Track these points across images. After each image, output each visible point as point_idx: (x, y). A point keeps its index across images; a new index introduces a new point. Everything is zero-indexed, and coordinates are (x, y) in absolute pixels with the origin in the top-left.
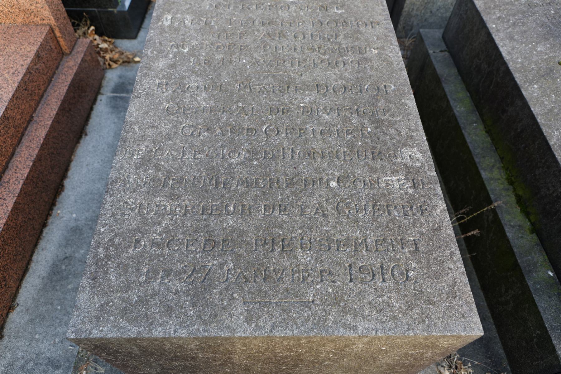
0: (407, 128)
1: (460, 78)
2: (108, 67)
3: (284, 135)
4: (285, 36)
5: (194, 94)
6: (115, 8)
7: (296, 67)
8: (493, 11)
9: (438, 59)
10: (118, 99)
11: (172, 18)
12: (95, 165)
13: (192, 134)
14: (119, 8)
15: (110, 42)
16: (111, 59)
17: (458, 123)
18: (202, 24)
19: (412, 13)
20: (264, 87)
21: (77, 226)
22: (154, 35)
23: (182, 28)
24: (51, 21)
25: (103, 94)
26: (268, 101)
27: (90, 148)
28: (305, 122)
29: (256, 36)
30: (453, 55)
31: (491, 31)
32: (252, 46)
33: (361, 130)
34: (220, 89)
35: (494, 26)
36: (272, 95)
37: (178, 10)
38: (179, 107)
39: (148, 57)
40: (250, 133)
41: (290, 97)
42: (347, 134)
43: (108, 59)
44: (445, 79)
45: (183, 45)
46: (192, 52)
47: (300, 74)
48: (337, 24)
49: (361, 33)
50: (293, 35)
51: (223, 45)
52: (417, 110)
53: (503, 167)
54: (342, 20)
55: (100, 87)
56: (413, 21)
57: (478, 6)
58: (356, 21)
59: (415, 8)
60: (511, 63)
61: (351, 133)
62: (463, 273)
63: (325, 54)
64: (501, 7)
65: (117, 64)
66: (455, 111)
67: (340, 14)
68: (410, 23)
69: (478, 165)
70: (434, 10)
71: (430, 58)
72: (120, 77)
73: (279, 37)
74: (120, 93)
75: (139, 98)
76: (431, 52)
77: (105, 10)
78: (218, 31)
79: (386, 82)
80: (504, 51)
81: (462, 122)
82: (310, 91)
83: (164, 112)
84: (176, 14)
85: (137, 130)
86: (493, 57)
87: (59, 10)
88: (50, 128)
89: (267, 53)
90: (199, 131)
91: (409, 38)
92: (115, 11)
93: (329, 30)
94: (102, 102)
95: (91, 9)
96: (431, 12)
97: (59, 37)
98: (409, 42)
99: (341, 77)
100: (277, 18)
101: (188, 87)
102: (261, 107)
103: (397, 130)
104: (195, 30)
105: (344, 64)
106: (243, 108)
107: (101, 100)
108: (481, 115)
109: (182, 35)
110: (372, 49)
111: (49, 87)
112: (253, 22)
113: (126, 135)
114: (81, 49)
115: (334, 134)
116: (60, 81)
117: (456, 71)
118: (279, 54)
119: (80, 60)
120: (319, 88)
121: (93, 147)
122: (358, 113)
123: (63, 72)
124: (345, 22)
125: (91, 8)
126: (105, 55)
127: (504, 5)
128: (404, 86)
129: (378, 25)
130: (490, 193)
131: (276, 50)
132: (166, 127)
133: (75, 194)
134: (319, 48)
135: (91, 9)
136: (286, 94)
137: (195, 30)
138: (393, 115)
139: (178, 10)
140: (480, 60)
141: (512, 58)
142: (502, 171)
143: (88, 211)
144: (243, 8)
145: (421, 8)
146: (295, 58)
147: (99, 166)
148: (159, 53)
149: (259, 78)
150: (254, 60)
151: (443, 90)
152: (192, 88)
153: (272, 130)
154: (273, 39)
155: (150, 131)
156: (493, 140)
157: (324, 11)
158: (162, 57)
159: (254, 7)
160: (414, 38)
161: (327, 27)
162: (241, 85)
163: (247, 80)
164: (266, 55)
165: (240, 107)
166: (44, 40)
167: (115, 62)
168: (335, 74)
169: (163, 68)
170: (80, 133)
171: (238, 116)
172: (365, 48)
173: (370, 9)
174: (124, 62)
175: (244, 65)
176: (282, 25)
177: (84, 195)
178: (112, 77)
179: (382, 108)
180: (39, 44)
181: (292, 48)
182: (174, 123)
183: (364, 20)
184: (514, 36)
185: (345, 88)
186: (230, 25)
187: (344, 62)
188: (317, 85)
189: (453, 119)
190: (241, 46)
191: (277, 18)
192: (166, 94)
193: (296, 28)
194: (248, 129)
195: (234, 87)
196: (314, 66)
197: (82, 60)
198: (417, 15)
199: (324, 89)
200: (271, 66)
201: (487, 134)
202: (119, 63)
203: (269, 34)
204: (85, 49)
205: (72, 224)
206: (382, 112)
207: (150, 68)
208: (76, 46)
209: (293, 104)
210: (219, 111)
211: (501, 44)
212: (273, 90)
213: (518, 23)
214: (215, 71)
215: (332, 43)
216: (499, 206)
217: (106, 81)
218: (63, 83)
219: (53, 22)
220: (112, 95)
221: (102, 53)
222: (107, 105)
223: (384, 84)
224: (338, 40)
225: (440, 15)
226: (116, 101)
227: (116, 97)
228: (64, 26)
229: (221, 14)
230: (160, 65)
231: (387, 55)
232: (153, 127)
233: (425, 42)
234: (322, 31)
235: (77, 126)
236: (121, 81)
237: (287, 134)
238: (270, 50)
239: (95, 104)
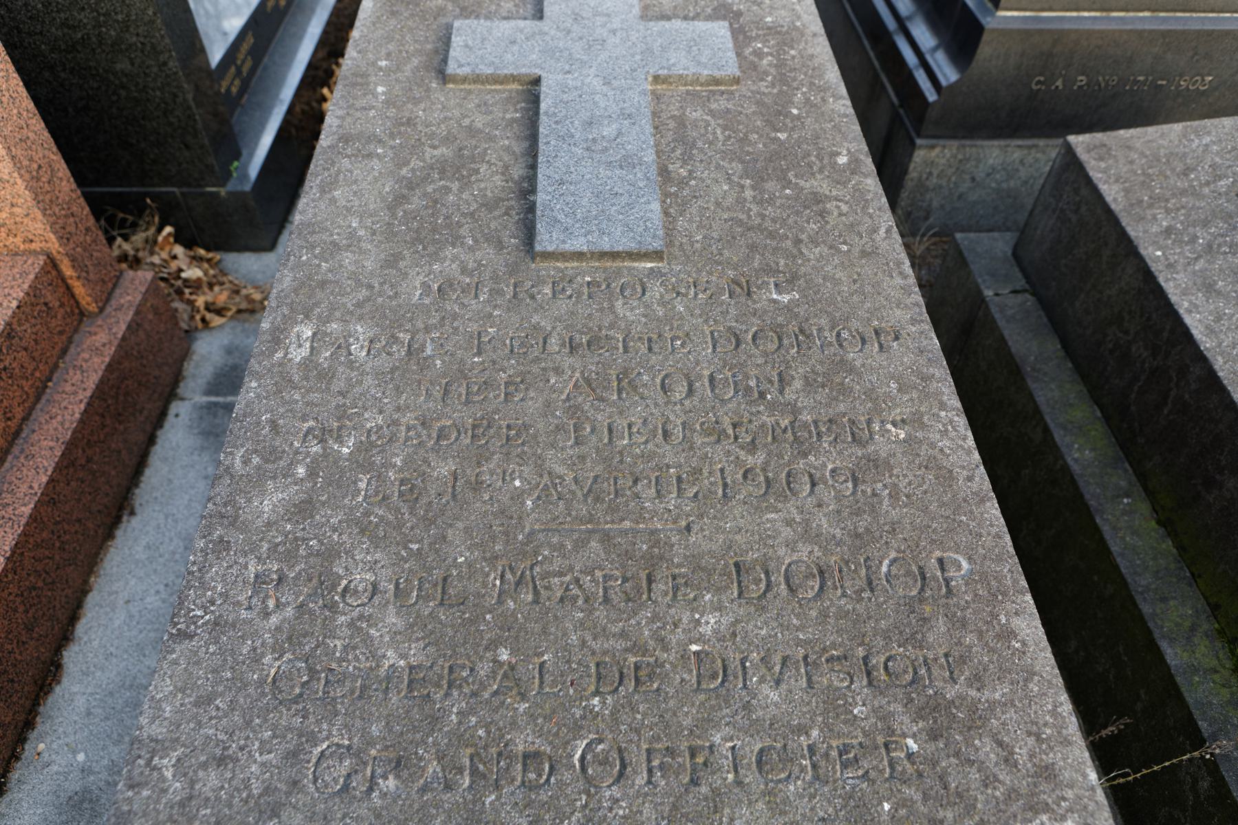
0: (1029, 734)
1: (1070, 365)
2: (200, 325)
3: (641, 780)
4: (635, 388)
5: (361, 617)
6: (223, 185)
7: (672, 501)
8: (1148, 212)
9: (1010, 312)
10: (220, 412)
11: (314, 334)
12: (148, 600)
13: (346, 788)
14: (232, 186)
15: (209, 261)
16: (208, 307)
17: (1082, 496)
18: (400, 352)
19: (928, 183)
20: (577, 580)
21: (86, 790)
22: (258, 396)
23: (341, 369)
24: (49, 245)
25: (182, 399)
26: (589, 638)
27: (140, 553)
28: (706, 723)
29: (553, 390)
30: (1046, 305)
31: (1154, 267)
32: (540, 426)
33: (886, 745)
34: (444, 592)
35: (1159, 253)
36: (601, 613)
37: (332, 308)
38: (312, 672)
39: (232, 477)
40: (532, 776)
41: (655, 618)
42: (845, 766)
43: (202, 308)
44: (1033, 369)
45: (340, 428)
46: (363, 459)
47: (684, 523)
48: (780, 339)
49: (851, 370)
50: (658, 381)
51: (454, 425)
52: (1049, 654)
53: (1221, 632)
54: (793, 327)
55: (177, 378)
56: (931, 200)
57: (1109, 199)
58: (832, 328)
59: (935, 173)
60: (1220, 360)
61: (856, 759)
62: (854, 166)
63: (752, 447)
64: (1167, 201)
65: (223, 316)
66: (1069, 460)
67: (788, 308)
68: (925, 205)
69: (1151, 625)
70: (980, 175)
71: (987, 307)
72: (229, 351)
73: (620, 391)
74: (225, 395)
75: (191, 637)
76: (988, 293)
77: (198, 190)
78: (444, 375)
79: (942, 546)
80: (1195, 323)
81: (1091, 491)
82: (719, 590)
83: (263, 694)
84: (328, 320)
85: (169, 774)
86: (1165, 334)
87: (73, 215)
88: (27, 524)
89: (584, 449)
90: (369, 772)
91: (923, 235)
92: (223, 192)
93: (760, 361)
94: (180, 418)
95: (164, 189)
96: (973, 179)
97: (71, 278)
98: (923, 247)
99: (809, 534)
100: (612, 326)
101: (346, 590)
102: (568, 662)
103: (1000, 744)
104: (378, 374)
105: (813, 485)
106: (512, 668)
107: (177, 415)
108: (1142, 477)
109: (340, 393)
110: (889, 426)
111: (39, 406)
112: (545, 343)
113: (129, 801)
114: (129, 298)
115: (803, 769)
116: (68, 388)
117: (1059, 346)
118: (621, 453)
119: (124, 327)
120: (744, 577)
121: (148, 547)
122: (869, 674)
123: (78, 363)
124: (802, 331)
125: (166, 186)
126: (193, 297)
127: (1174, 195)
128: (999, 559)
129: (897, 338)
130: (1197, 714)
131: (610, 439)
132: (266, 757)
133: (89, 690)
134: (735, 426)
135: (164, 189)
136: (643, 606)
137: (378, 374)
138: (977, 680)
139: (332, 308)
140: (1126, 333)
141: (1220, 345)
142: (1218, 644)
143: (117, 743)
144: (515, 295)
145: (950, 171)
146: (668, 467)
147: (159, 603)
148: (267, 461)
149: (562, 546)
150: (546, 478)
151: (1031, 397)
152: (356, 591)
153: (604, 762)
154: (602, 399)
155: (211, 779)
156: (1181, 548)
157: (743, 299)
158: (274, 478)
159: (547, 290)
160: (934, 235)
161: (755, 351)
162: (509, 576)
163: (525, 554)
164: (582, 458)
165: (501, 664)
166: (28, 294)
167: (219, 312)
168: (789, 523)
169: (273, 518)
170: (119, 507)
171: (496, 702)
172: (869, 422)
173: (868, 289)
174: (239, 311)
175: (518, 496)
176: (626, 350)
177: (111, 694)
178: (209, 350)
179: (941, 652)
180: (14, 304)
181: (656, 427)
182: (292, 740)
183: (855, 324)
184: (1215, 283)
185: (821, 572)
186: (479, 354)
187: (811, 476)
188: (737, 565)
189: (1063, 477)
190: (509, 427)
191: (612, 326)
192: (274, 620)
193: (667, 359)
194: (526, 756)
195: (485, 585)
196: (725, 495)
197: (129, 327)
198: (941, 187)
199: (757, 581)
200: (597, 499)
201: (1162, 531)
202: (229, 314)
203: (588, 381)
204: (139, 297)
205: (74, 785)
206: (942, 667)
207: (237, 517)
208: (118, 291)
209: (665, 649)
210: (438, 685)
211: (1186, 304)
212: (605, 590)
213: (1219, 246)
214: (429, 522)
215: (772, 407)
216: (1226, 757)
217: (192, 364)
218: (75, 393)
219: (54, 245)
220: (205, 399)
221: (187, 291)
222: (190, 427)
223: (938, 554)
224: (789, 395)
225: (993, 185)
226: (215, 416)
227: (216, 404)
228: (85, 250)
229: (455, 317)
230: (267, 506)
231: (933, 445)
232: (221, 761)
233: (972, 267)
234: (742, 365)
235: (107, 495)
236: (231, 362)
237: (650, 771)
238: (594, 438)
239: (161, 427)
